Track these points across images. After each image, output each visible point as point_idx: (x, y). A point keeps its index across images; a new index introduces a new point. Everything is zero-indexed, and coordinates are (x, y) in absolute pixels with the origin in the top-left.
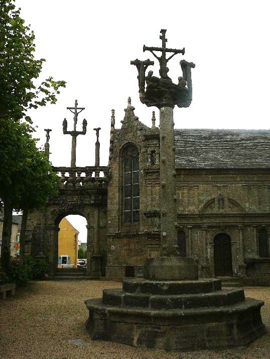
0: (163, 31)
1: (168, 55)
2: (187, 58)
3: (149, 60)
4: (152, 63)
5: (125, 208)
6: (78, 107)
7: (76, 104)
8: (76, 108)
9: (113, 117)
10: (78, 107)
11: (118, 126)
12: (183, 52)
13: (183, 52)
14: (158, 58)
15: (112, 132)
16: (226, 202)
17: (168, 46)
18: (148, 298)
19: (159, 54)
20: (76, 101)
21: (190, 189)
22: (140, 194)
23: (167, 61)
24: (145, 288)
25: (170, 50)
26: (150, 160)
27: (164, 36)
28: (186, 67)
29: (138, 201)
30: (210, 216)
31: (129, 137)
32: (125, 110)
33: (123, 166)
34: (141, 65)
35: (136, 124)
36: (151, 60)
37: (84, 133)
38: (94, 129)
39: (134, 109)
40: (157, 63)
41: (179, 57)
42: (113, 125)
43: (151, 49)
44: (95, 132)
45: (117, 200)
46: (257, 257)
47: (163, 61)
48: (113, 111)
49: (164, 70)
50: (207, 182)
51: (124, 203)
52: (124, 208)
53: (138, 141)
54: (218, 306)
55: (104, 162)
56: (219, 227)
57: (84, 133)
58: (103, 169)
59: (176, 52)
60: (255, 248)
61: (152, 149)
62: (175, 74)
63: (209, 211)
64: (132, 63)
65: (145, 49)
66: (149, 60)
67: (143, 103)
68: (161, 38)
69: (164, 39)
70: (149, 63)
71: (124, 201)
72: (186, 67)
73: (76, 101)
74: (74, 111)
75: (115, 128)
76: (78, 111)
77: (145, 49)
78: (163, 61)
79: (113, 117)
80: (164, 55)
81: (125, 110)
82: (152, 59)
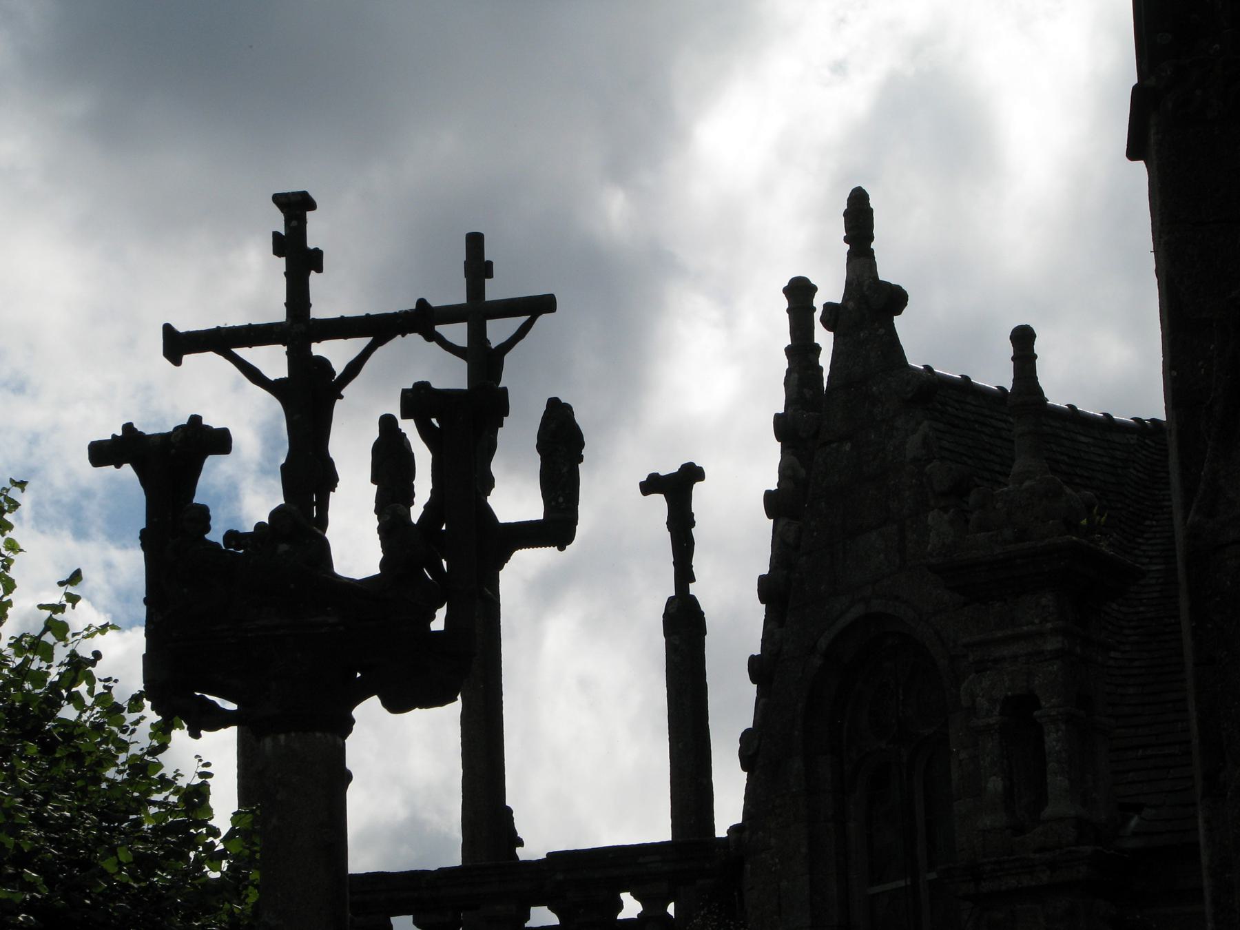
0: (295, 206)
3: (195, 420)
6: (494, 291)
7: (478, 267)
8: (477, 311)
10: (494, 291)
20: (475, 242)
23: (431, 336)
34: (167, 462)
36: (213, 420)
37: (556, 528)
38: (651, 485)
43: (222, 341)
44: (659, 503)
47: (308, 400)
49: (308, 475)
57: (556, 528)
65: (178, 345)
66: (195, 420)
69: (299, 258)
70: (201, 441)
73: (475, 242)
74: (457, 333)
76: (498, 331)
78: (308, 400)
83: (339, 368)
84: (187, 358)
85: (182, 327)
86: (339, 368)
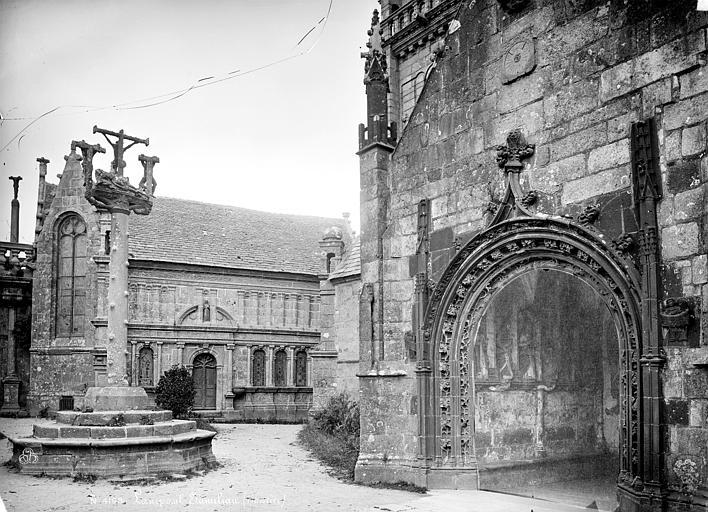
1: (126, 143)
11: (52, 179)
12: (146, 143)
13: (146, 143)
16: (214, 314)
19: (114, 140)
21: (164, 290)
24: (82, 421)
25: (130, 138)
28: (148, 162)
30: (187, 330)
34: (89, 151)
36: (102, 146)
40: (110, 151)
41: (139, 149)
43: (104, 132)
46: (249, 386)
47: (118, 149)
49: (118, 164)
50: (188, 284)
55: (27, 236)
56: (200, 345)
58: (23, 248)
59: (136, 141)
60: (248, 373)
62: (133, 174)
63: (188, 323)
65: (96, 130)
72: (148, 162)
75: (47, 180)
77: (96, 130)
78: (118, 149)
80: (120, 143)
82: (105, 145)
86: (125, 146)
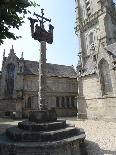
2: (52, 23)
4: (38, 22)
5: (7, 88)
9: (4, 52)
11: (7, 56)
12: (50, 21)
13: (50, 21)
14: (40, 21)
15: (3, 58)
17: (44, 16)
18: (40, 134)
22: (14, 83)
25: (45, 19)
26: (20, 70)
27: (43, 11)
29: (13, 85)
31: (12, 61)
32: (10, 50)
33: (8, 71)
35: (14, 56)
39: (14, 50)
42: (4, 55)
43: (37, 15)
45: (4, 85)
48: (4, 50)
51: (7, 86)
52: (7, 88)
53: (15, 62)
54: (55, 134)
59: (47, 20)
61: (21, 66)
64: (18, 29)
67: (33, 38)
68: (41, 12)
70: (36, 21)
71: (7, 85)
72: (51, 27)
79: (4, 52)
81: (10, 50)
83: (44, 21)
84: (35, 15)
85: (35, 13)
86: (44, 21)
